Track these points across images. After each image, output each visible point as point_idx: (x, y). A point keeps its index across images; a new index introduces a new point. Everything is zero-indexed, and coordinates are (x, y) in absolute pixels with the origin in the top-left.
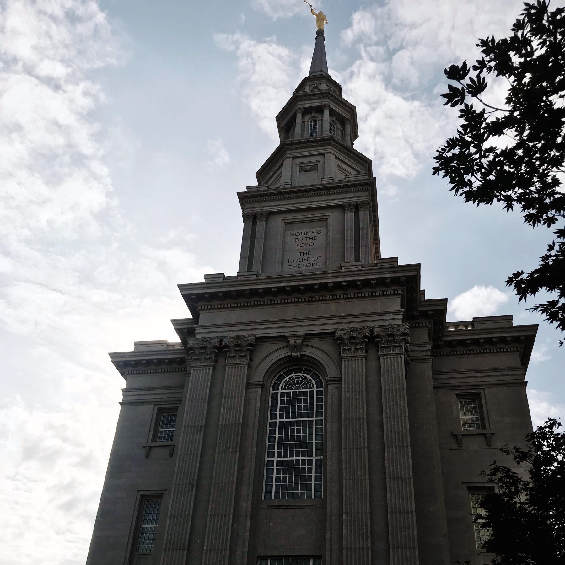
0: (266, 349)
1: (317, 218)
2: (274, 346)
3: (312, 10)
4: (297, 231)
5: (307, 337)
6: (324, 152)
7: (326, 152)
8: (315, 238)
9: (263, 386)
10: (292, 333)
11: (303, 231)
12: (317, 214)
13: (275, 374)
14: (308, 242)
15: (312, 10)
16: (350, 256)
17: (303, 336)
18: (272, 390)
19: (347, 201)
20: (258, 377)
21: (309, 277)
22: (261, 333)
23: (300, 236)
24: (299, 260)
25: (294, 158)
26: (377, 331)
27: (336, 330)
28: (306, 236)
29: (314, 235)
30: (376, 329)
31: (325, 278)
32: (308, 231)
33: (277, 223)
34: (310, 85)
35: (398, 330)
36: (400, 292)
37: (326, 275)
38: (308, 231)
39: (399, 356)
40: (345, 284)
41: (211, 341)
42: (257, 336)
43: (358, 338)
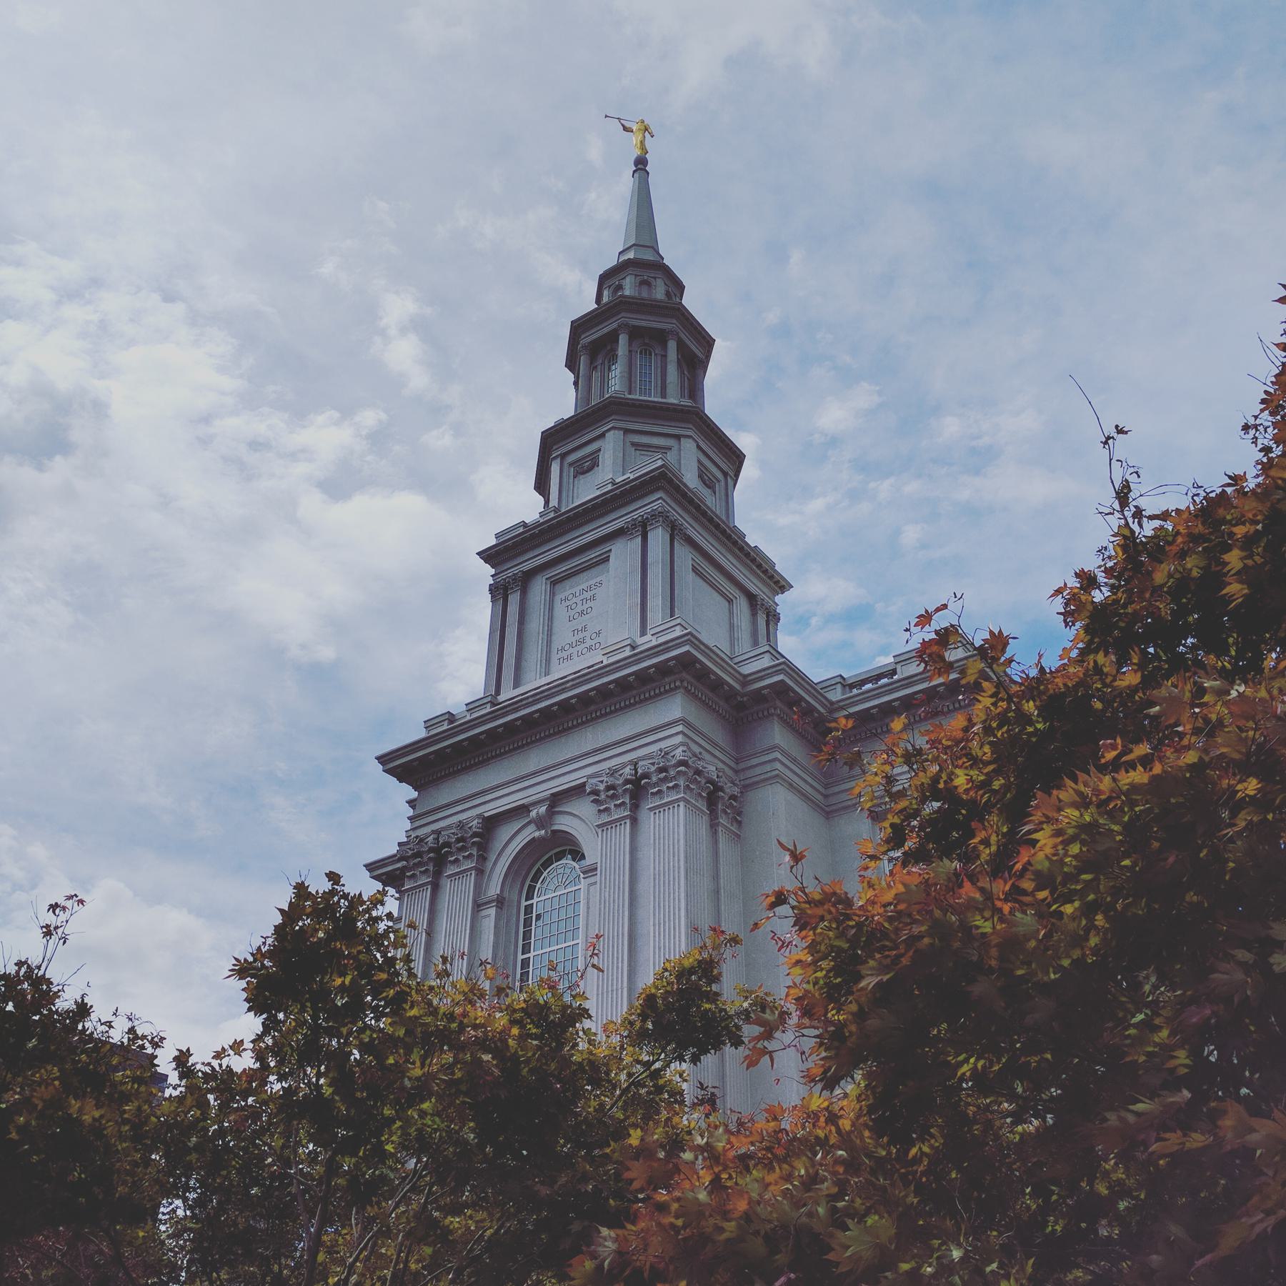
0: (505, 832)
1: (595, 560)
2: (517, 825)
3: (623, 125)
4: (570, 592)
5: (556, 800)
6: (603, 430)
7: (606, 429)
8: (593, 598)
9: (500, 902)
10: (534, 797)
11: (577, 590)
12: (593, 554)
13: (524, 873)
14: (586, 606)
15: (623, 125)
16: (656, 613)
17: (547, 798)
18: (526, 901)
19: (628, 518)
20: (494, 889)
21: (541, 695)
22: (490, 809)
23: (575, 600)
24: (571, 645)
25: (563, 456)
26: (643, 767)
27: (589, 777)
28: (582, 597)
29: (593, 592)
30: (641, 763)
31: (563, 691)
32: (584, 586)
33: (539, 587)
34: (610, 287)
35: (621, 775)
36: (678, 683)
37: (564, 687)
38: (584, 586)
39: (676, 805)
40: (611, 686)
41: (621, 772)
42: (486, 815)
43: (619, 785)
